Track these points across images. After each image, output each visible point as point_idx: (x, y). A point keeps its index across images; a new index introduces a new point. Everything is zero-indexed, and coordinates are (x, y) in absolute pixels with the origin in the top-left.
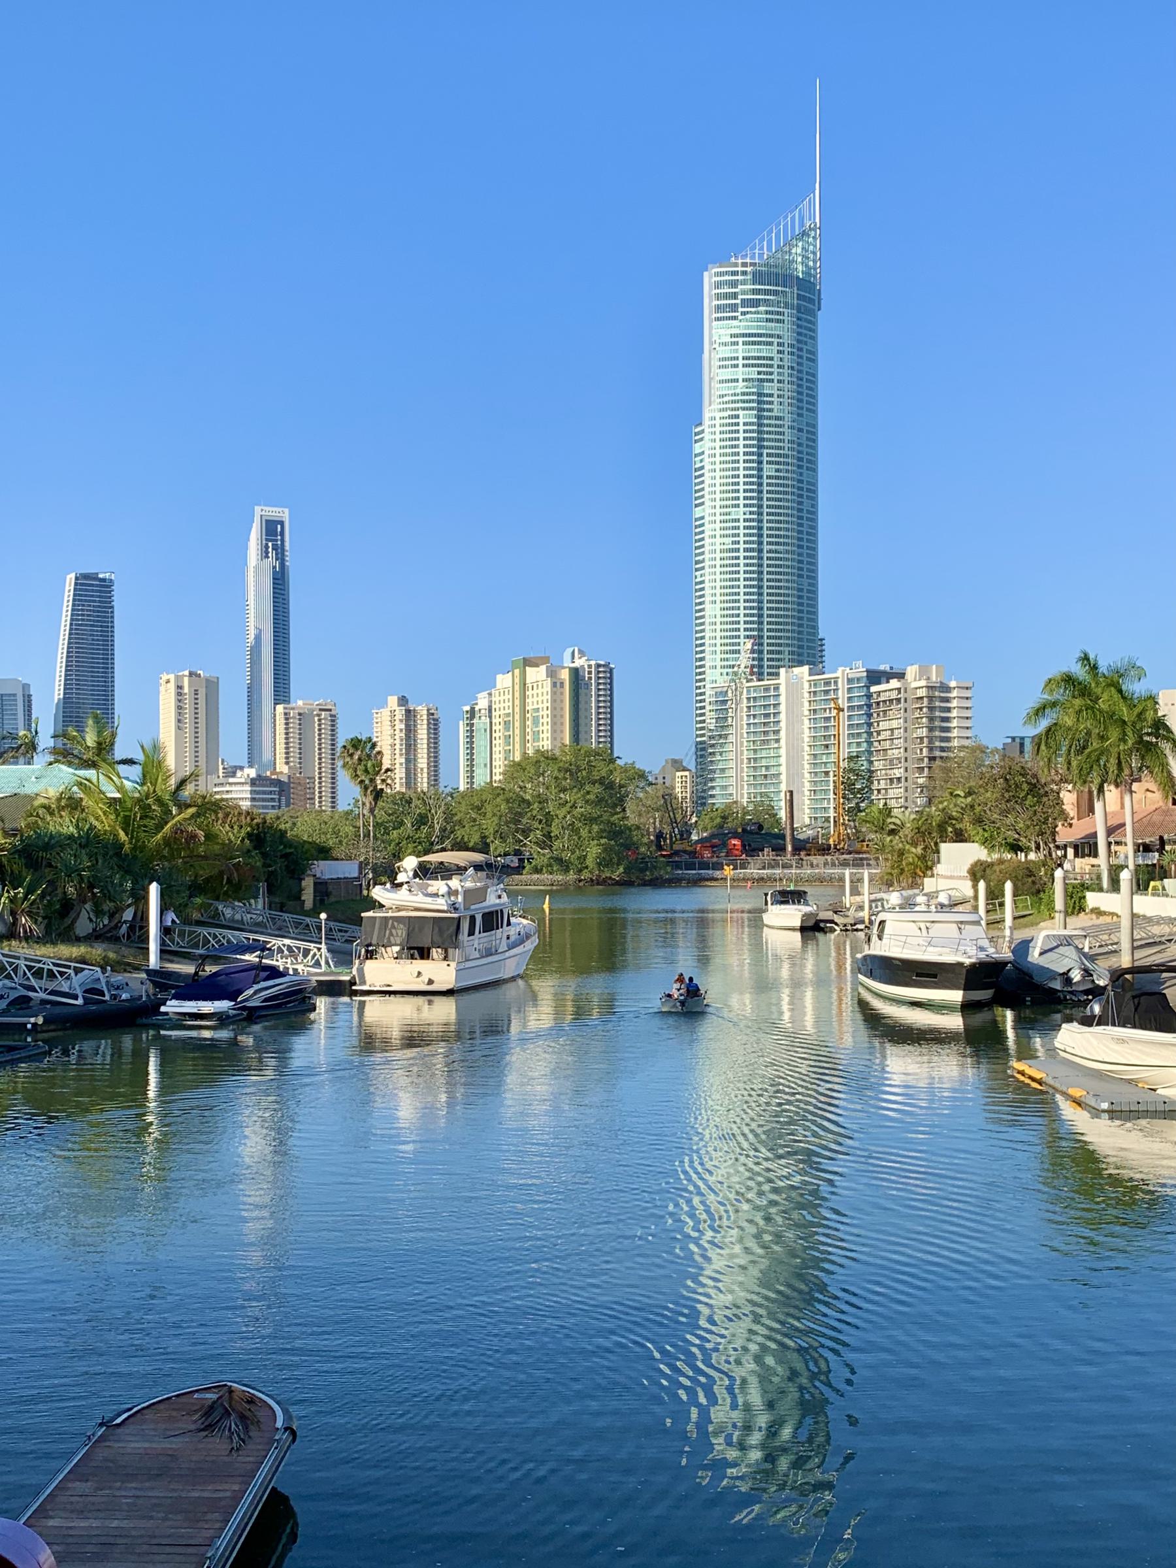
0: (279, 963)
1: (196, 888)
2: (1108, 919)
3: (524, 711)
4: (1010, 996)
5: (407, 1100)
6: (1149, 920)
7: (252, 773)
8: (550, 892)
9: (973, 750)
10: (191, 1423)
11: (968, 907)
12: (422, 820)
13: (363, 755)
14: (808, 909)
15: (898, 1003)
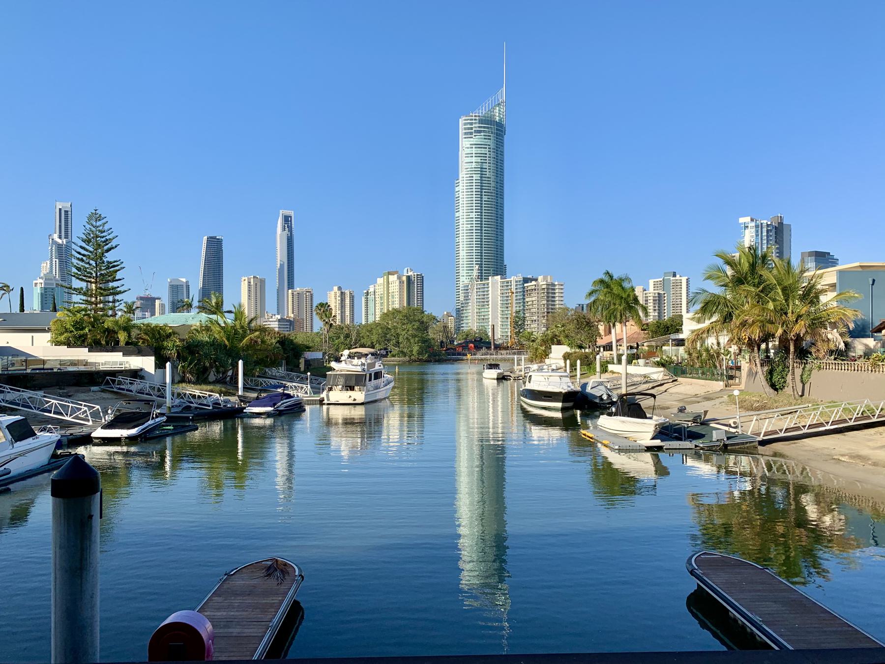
0: (291, 392)
1: (257, 363)
2: (616, 375)
3: (388, 293)
4: (580, 406)
5: (343, 444)
6: (632, 375)
7: (279, 317)
8: (398, 365)
9: (563, 309)
10: (263, 573)
11: (562, 370)
12: (347, 336)
13: (324, 308)
14: (499, 371)
15: (536, 407)
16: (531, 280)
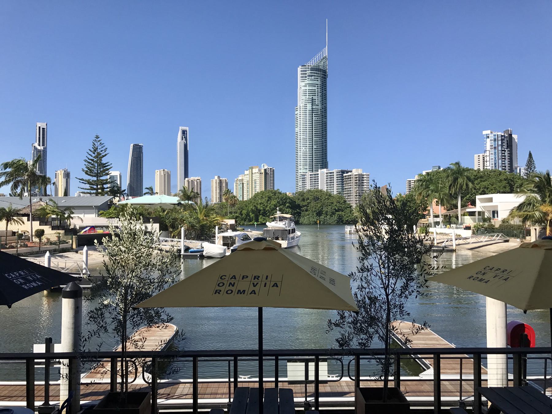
16: (347, 172)
